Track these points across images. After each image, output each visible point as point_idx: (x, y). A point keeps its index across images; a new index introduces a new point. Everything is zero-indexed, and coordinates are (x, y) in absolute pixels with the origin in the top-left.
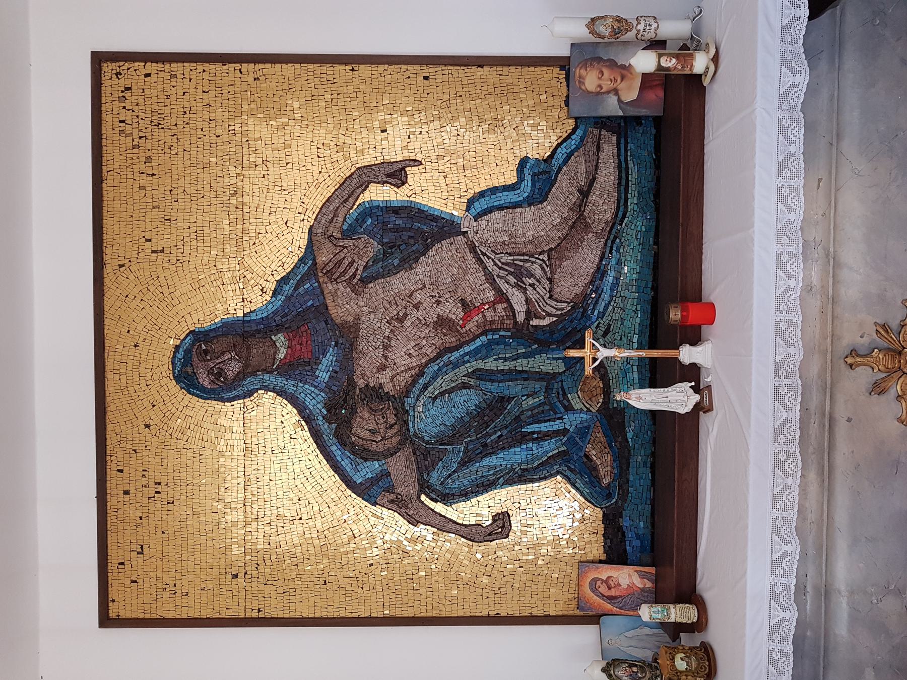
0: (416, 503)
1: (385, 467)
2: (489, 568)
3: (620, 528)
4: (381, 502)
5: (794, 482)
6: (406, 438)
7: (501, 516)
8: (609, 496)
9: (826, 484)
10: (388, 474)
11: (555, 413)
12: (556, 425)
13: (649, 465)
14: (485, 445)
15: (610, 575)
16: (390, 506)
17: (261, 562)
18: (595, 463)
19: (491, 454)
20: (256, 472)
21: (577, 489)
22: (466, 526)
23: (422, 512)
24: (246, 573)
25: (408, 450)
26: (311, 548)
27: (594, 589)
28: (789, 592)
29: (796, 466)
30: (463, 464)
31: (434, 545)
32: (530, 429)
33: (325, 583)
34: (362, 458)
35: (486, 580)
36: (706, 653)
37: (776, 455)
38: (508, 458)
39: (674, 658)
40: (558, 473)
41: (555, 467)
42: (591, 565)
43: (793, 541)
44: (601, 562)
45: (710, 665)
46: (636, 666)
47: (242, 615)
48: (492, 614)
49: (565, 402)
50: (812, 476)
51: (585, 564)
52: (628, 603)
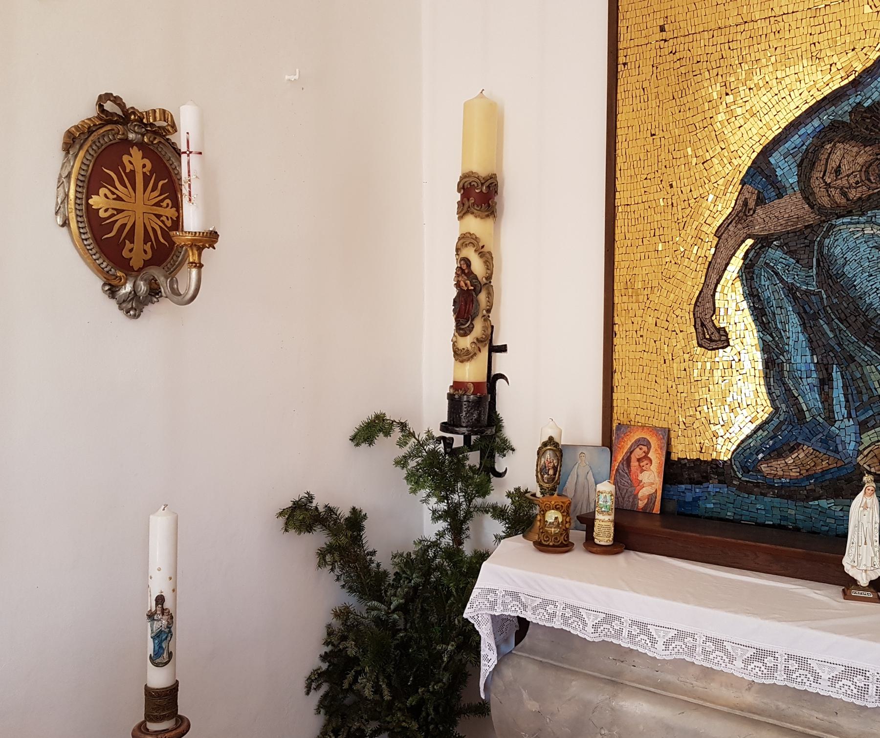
0: (742, 233)
1: (790, 191)
2: (665, 325)
3: (707, 479)
4: (745, 191)
5: (737, 668)
6: (827, 217)
7: (723, 338)
8: (746, 470)
9: (738, 713)
10: (780, 196)
11: (856, 410)
12: (840, 410)
13: (783, 523)
14: (815, 317)
15: (653, 462)
16: (740, 202)
17: (678, 56)
18: (787, 456)
19: (803, 324)
20: (787, 28)
21: (755, 431)
22: (713, 296)
23: (731, 242)
24: (665, 41)
25: (811, 218)
26: (691, 113)
27: (640, 443)
28: (613, 637)
29: (756, 675)
30: (791, 291)
31: (692, 259)
32: (836, 375)
33: (652, 135)
34: (802, 161)
35: (651, 320)
36: (562, 546)
37: (772, 654)
38: (798, 346)
39: (557, 509)
40: (776, 409)
41: (783, 406)
42: (665, 441)
43: (668, 652)
44: (668, 454)
45: (548, 546)
46: (555, 474)
47: (620, 46)
48: (616, 328)
49: (872, 423)
50: (750, 698)
51: (666, 435)
52: (623, 476)
